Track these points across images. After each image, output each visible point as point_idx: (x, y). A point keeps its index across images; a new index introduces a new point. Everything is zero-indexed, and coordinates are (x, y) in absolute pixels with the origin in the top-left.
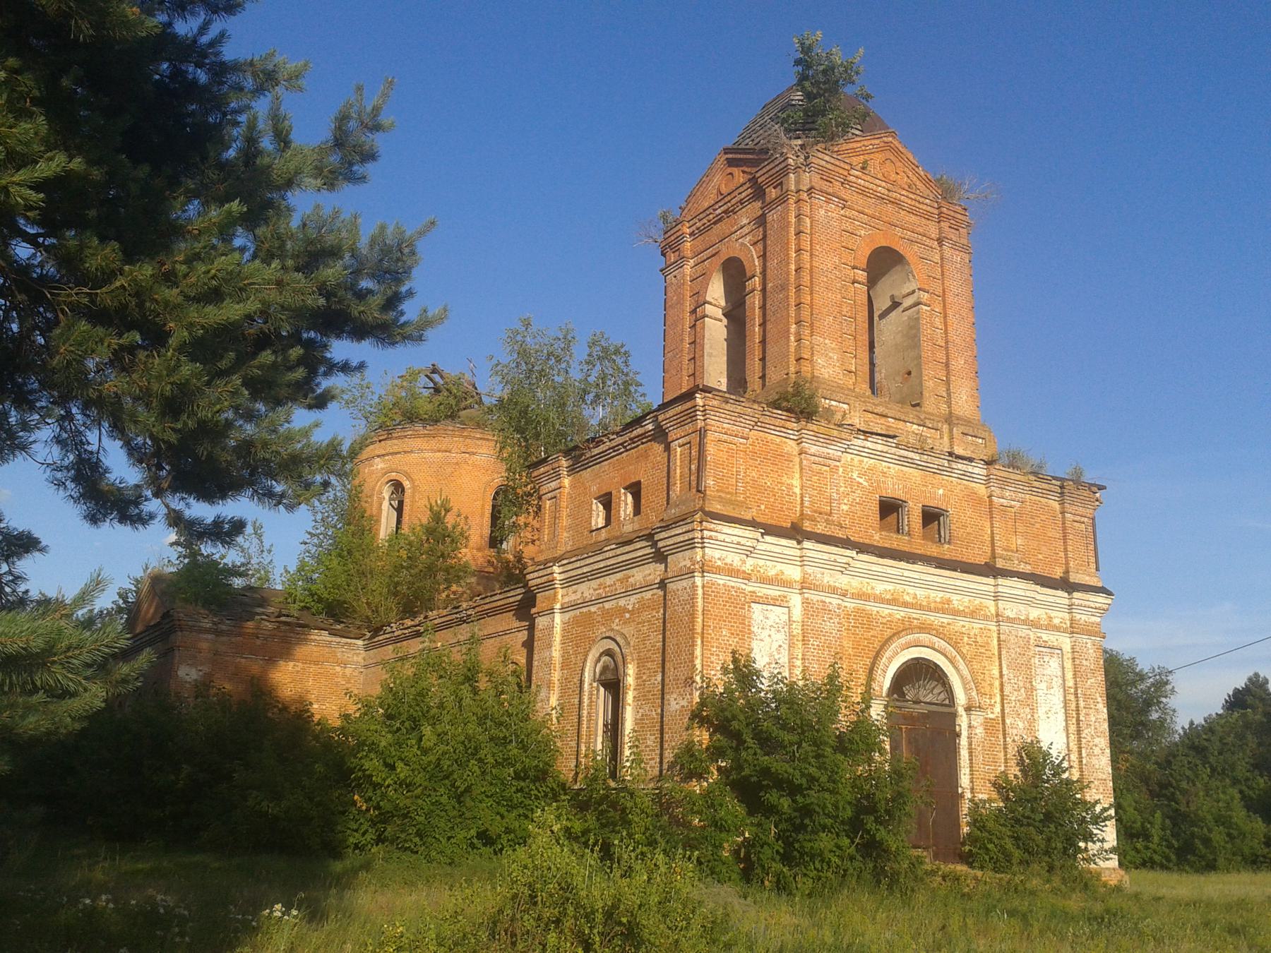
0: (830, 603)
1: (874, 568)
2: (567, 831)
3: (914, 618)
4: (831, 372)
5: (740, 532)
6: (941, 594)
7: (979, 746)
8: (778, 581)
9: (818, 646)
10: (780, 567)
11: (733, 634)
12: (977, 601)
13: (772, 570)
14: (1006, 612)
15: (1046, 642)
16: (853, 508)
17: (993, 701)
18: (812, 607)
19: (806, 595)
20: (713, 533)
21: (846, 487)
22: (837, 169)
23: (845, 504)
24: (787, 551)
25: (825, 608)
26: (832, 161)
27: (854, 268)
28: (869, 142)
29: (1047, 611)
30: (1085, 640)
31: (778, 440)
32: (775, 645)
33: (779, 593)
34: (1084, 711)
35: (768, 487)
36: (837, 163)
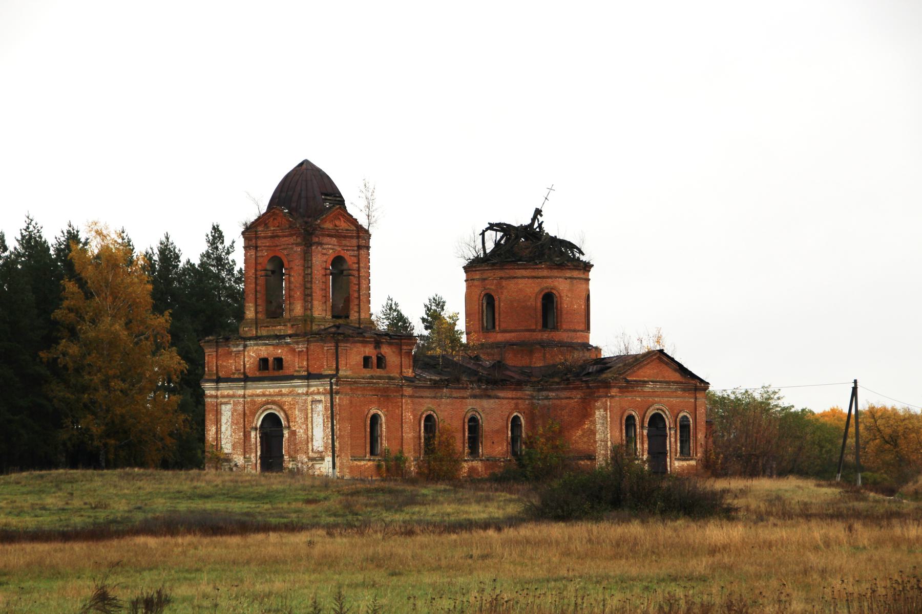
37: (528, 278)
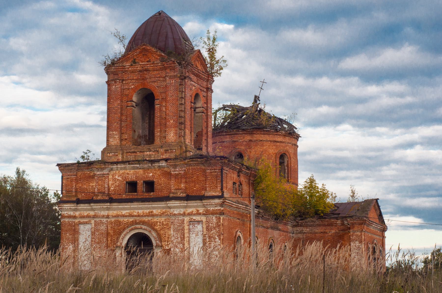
2: (392, 266)
3: (137, 220)
4: (115, 142)
5: (70, 205)
6: (148, 210)
9: (98, 234)
14: (174, 212)
16: (115, 188)
18: (97, 223)
20: (62, 207)
21: (113, 182)
23: (112, 187)
29: (196, 208)
32: (88, 236)
33: (88, 220)
34: (209, 243)
35: (85, 188)
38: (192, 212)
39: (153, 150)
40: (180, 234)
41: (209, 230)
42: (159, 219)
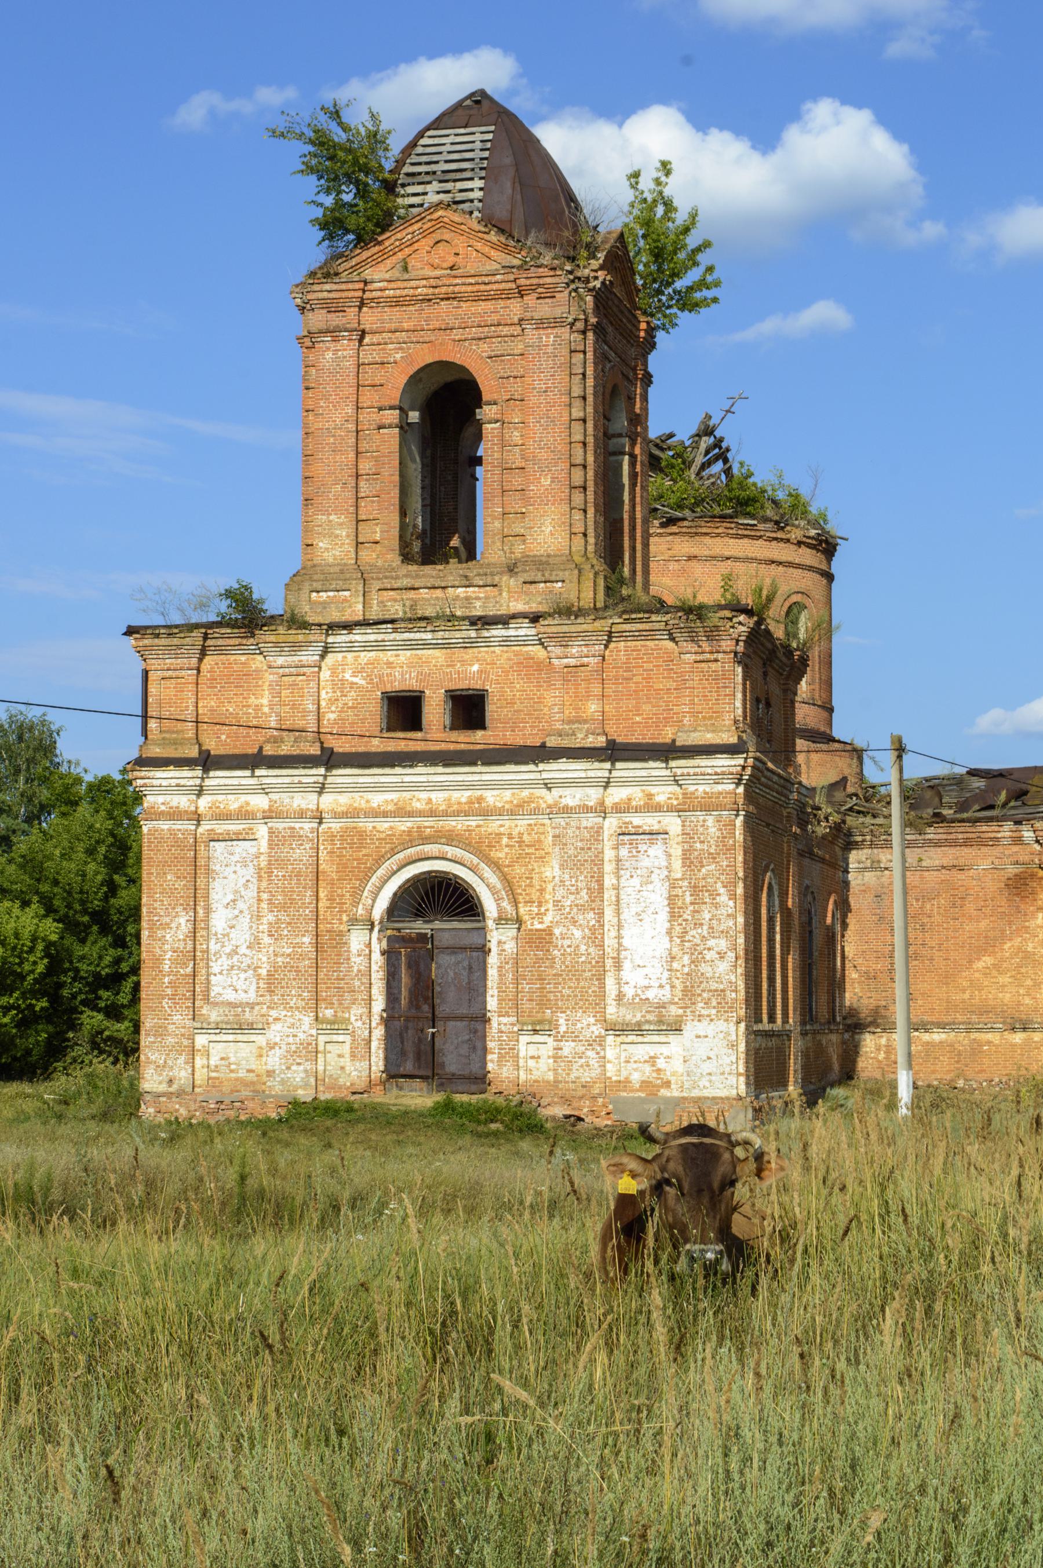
0: (301, 828)
1: (361, 780)
5: (177, 774)
7: (507, 963)
8: (244, 814)
9: (284, 876)
10: (243, 798)
11: (178, 877)
12: (525, 793)
13: (234, 803)
15: (639, 827)
16: (343, 715)
17: (543, 909)
19: (270, 825)
22: (346, 294)
24: (244, 781)
25: (294, 835)
26: (335, 287)
27: (380, 409)
28: (404, 233)
30: (702, 818)
31: (243, 658)
35: (231, 714)
36: (343, 287)
37: (760, 561)
38: (629, 799)
39: (481, 583)
40: (586, 877)
41: (692, 862)
42: (507, 823)
